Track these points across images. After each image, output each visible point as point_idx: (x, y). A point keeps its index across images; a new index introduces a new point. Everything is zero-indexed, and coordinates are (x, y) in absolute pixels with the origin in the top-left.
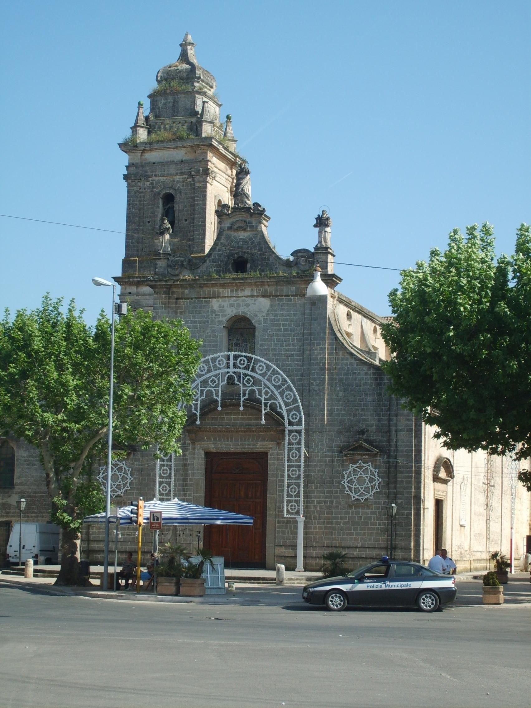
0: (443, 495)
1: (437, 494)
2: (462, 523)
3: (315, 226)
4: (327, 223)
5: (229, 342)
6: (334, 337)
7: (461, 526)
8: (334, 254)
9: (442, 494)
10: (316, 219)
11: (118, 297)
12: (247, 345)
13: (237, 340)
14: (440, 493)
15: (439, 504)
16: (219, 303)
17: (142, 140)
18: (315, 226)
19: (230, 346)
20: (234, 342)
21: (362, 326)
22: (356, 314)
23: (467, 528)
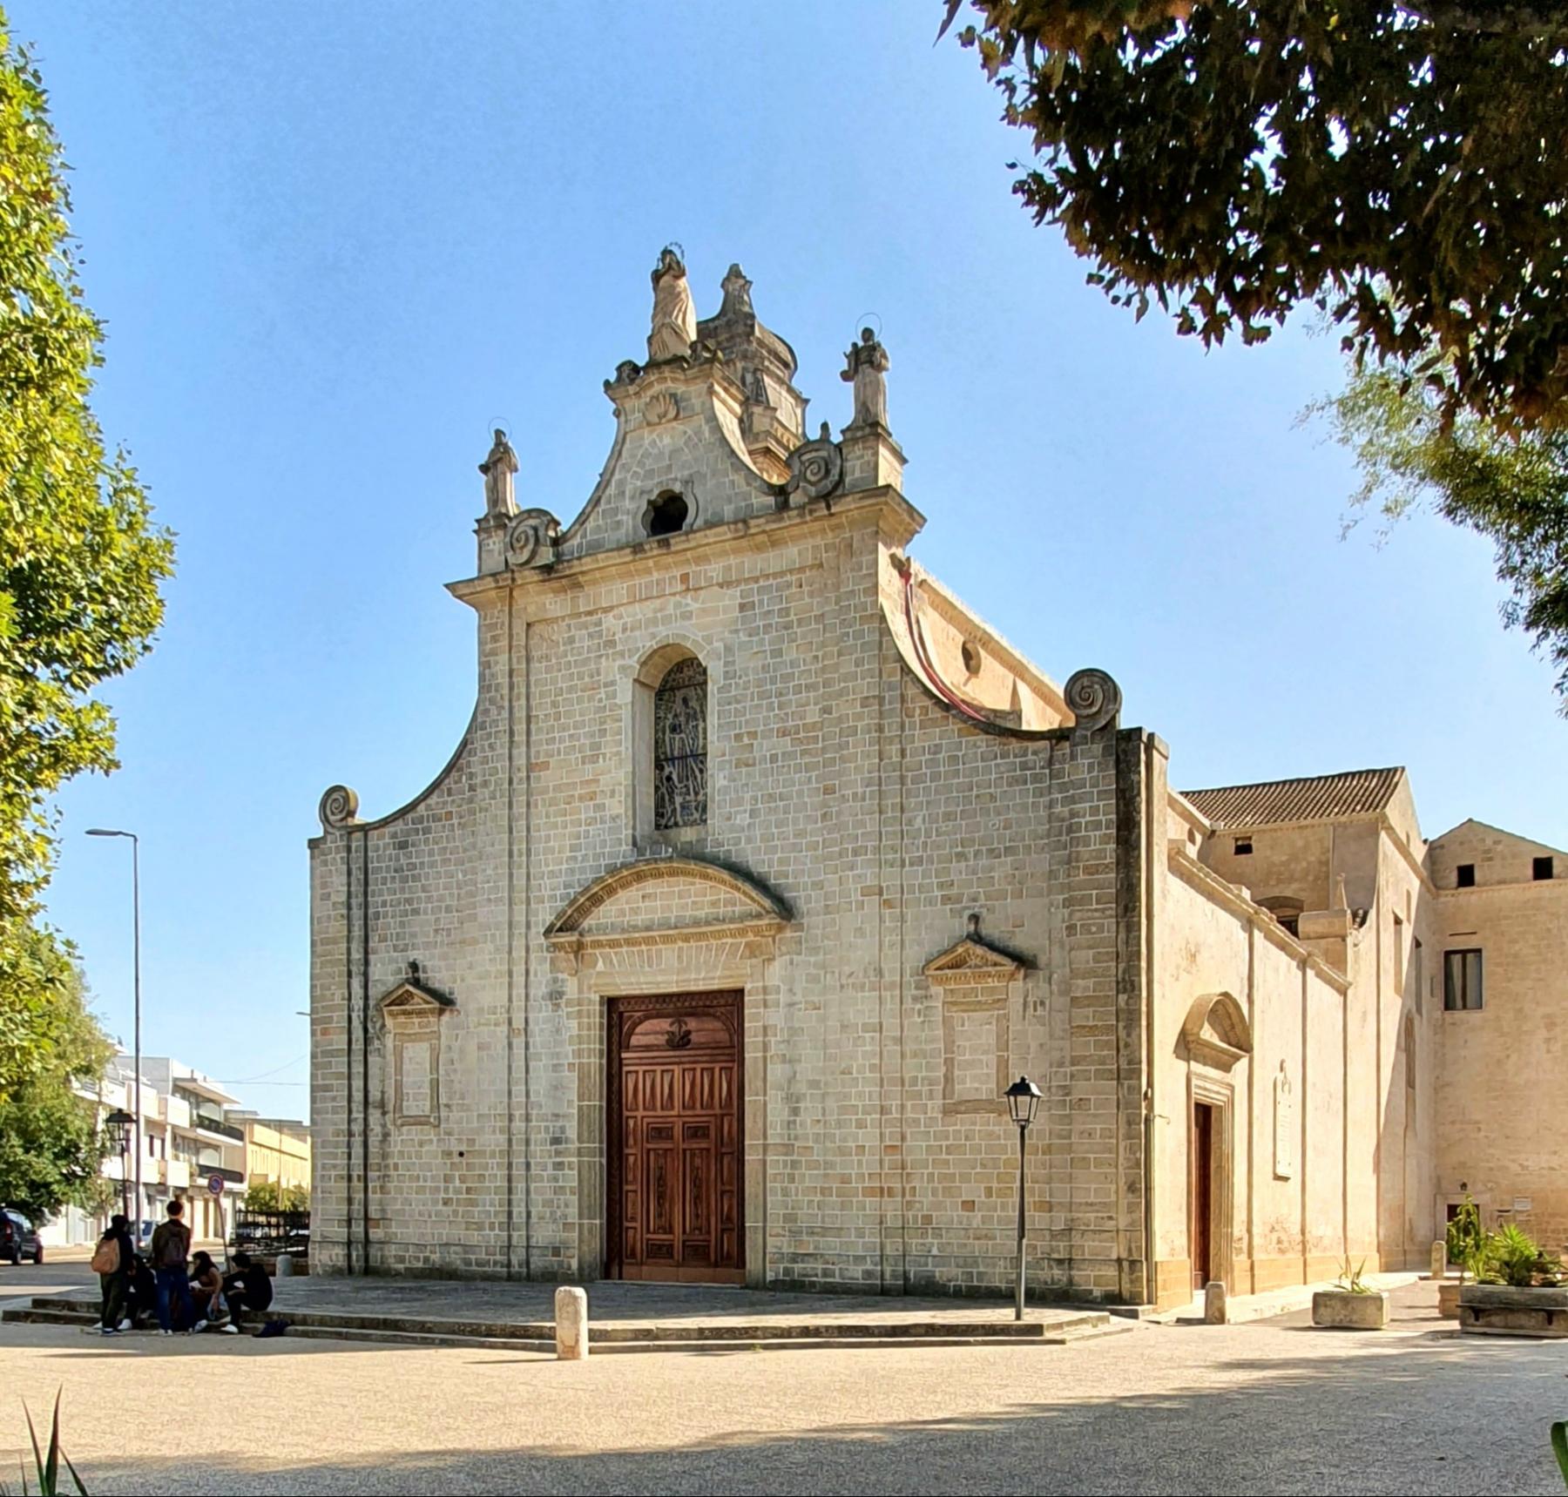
0: (1218, 1093)
1: (1198, 1087)
2: (1280, 1172)
3: (846, 376)
4: (1455, 1264)
5: (657, 724)
6: (898, 665)
7: (1278, 1178)
8: (905, 454)
9: (1216, 1088)
10: (847, 356)
11: (475, 536)
12: (697, 726)
13: (676, 716)
14: (1208, 1086)
15: (1205, 1119)
16: (622, 621)
17: (1303, 308)
18: (846, 376)
19: (660, 734)
20: (668, 723)
21: (1243, 1324)
22: (990, 659)
23: (1295, 1184)
